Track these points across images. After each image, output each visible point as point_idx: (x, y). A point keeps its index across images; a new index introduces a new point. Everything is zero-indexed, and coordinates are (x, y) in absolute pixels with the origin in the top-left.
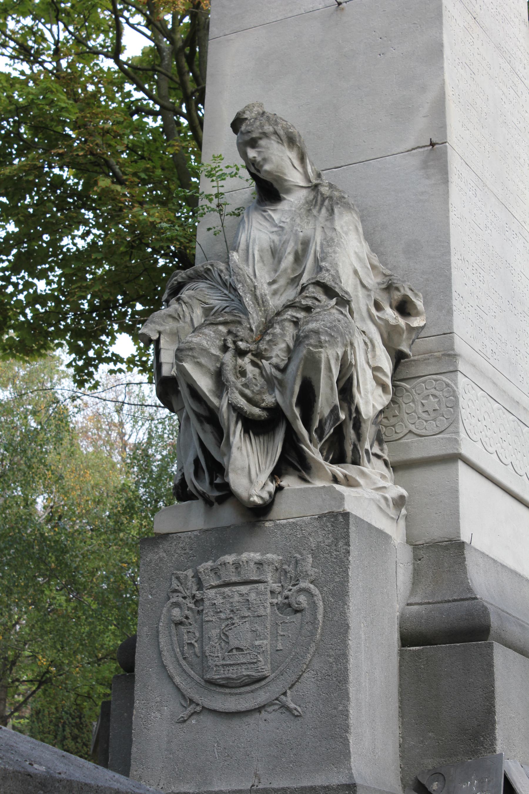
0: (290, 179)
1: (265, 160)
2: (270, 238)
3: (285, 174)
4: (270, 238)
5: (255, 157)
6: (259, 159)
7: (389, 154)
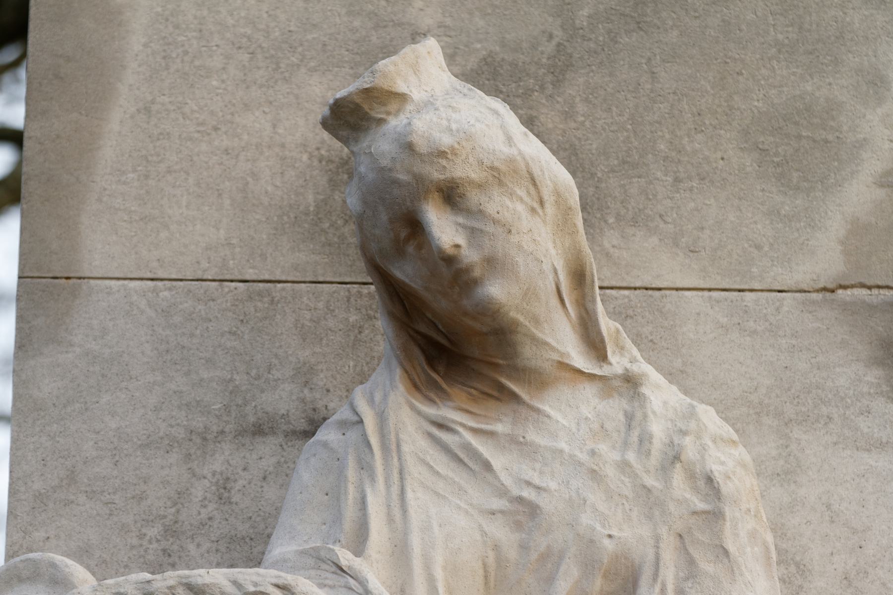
0: (550, 340)
1: (491, 262)
2: (484, 534)
3: (536, 321)
4: (484, 534)
5: (457, 246)
6: (470, 256)
7: (757, 286)
